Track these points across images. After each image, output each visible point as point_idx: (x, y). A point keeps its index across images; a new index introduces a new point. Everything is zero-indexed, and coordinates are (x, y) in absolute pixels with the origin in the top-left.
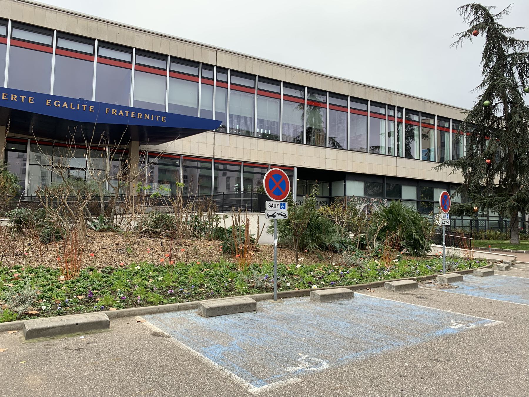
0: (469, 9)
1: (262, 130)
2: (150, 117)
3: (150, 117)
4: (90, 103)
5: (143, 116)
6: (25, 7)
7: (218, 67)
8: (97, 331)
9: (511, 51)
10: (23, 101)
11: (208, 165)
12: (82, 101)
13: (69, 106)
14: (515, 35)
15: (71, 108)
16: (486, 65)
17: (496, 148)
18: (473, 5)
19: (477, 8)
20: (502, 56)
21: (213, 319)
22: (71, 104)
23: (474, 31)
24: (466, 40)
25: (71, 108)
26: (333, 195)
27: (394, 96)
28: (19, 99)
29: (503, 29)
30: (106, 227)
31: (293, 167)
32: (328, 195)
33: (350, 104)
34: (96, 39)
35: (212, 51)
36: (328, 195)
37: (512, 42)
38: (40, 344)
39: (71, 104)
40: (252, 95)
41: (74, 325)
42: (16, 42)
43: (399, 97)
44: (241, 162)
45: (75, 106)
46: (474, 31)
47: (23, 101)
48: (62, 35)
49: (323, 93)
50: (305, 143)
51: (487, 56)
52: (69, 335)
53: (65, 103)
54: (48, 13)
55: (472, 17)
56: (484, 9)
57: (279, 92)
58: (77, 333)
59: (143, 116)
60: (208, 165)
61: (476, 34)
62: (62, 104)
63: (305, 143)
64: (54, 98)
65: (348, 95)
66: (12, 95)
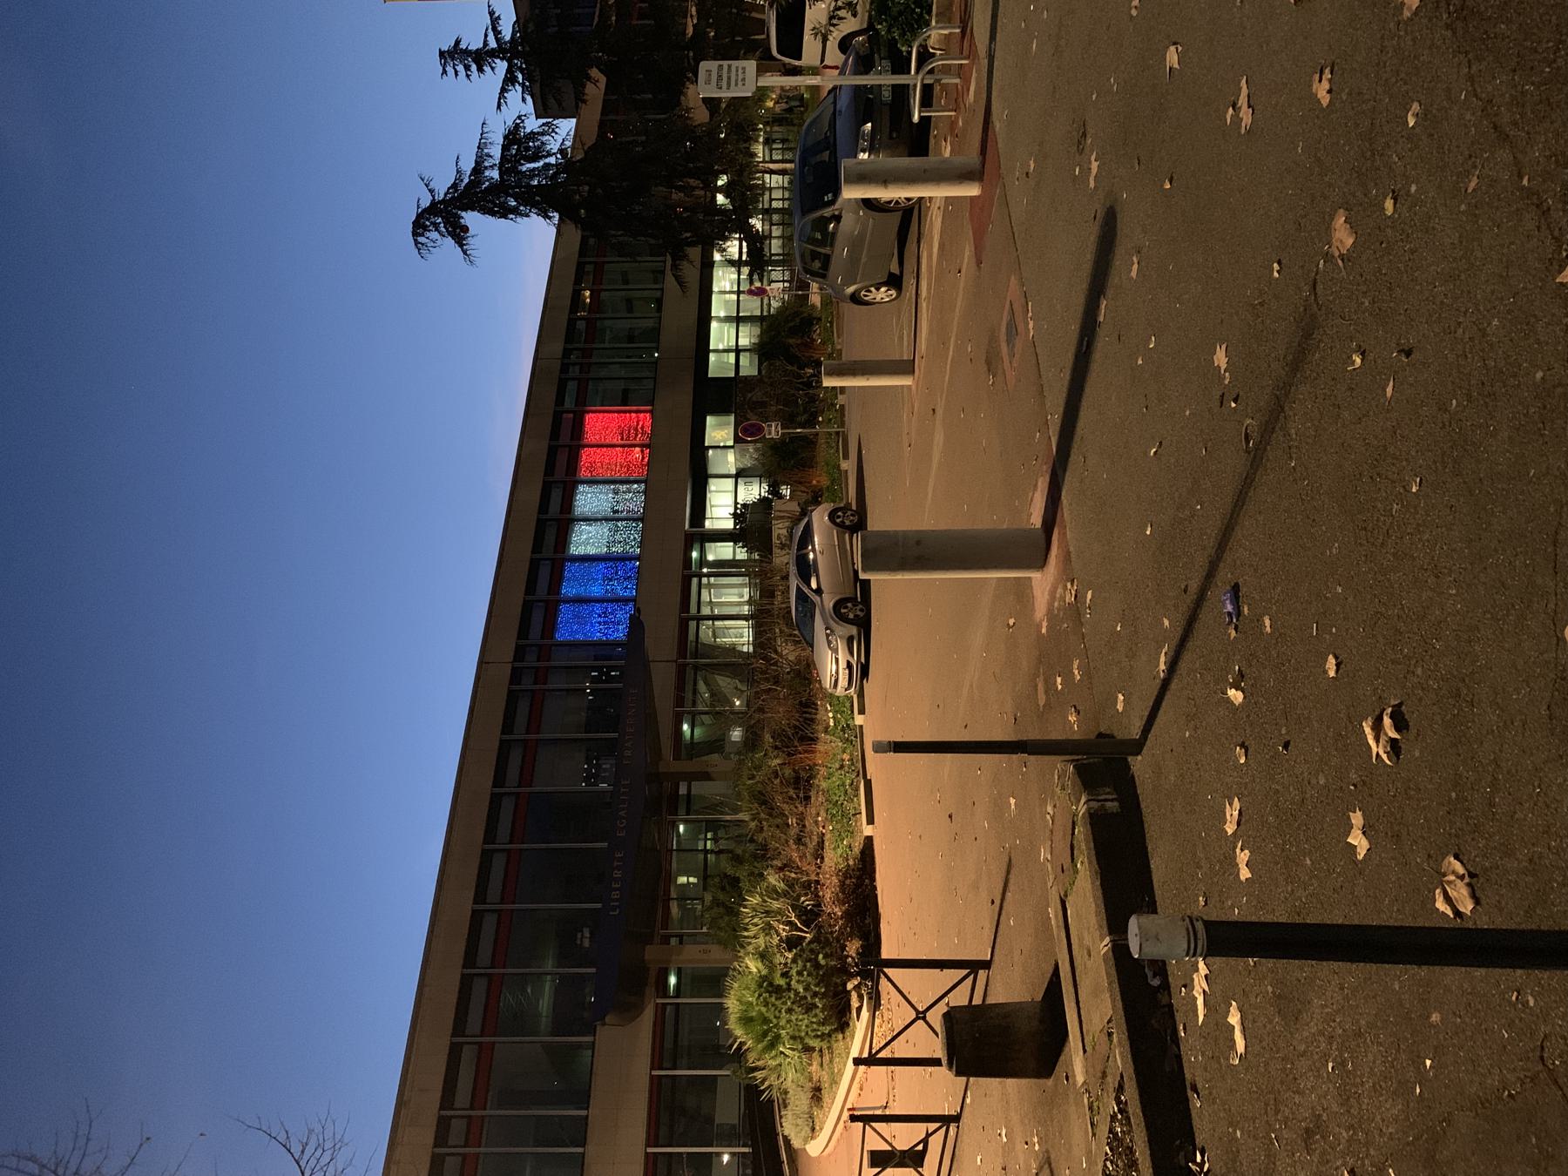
0: (421, 239)
9: (495, 174)
14: (468, 165)
16: (515, 211)
17: (549, 130)
18: (415, 234)
19: (419, 227)
20: (499, 188)
21: (913, 159)
23: (459, 234)
24: (472, 243)
26: (734, 472)
29: (454, 186)
30: (853, 948)
32: (731, 482)
36: (731, 482)
37: (478, 170)
46: (459, 234)
51: (504, 212)
55: (434, 235)
56: (419, 216)
61: (466, 229)
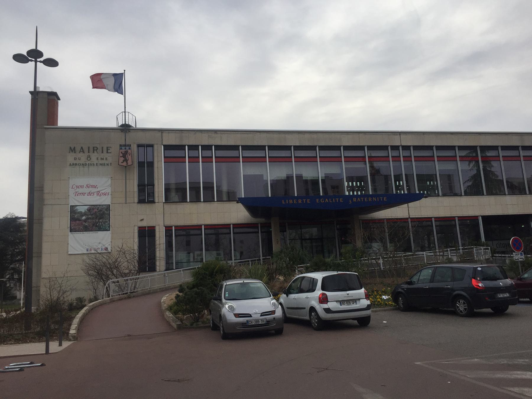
1: (359, 194)
2: (377, 199)
3: (377, 199)
5: (372, 199)
7: (403, 147)
13: (329, 201)
27: (398, 137)
31: (478, 216)
33: (522, 153)
34: (212, 146)
35: (397, 135)
40: (455, 162)
42: (505, 158)
43: (403, 136)
48: (297, 148)
49: (495, 148)
50: (485, 193)
57: (409, 155)
59: (372, 199)
63: (485, 193)
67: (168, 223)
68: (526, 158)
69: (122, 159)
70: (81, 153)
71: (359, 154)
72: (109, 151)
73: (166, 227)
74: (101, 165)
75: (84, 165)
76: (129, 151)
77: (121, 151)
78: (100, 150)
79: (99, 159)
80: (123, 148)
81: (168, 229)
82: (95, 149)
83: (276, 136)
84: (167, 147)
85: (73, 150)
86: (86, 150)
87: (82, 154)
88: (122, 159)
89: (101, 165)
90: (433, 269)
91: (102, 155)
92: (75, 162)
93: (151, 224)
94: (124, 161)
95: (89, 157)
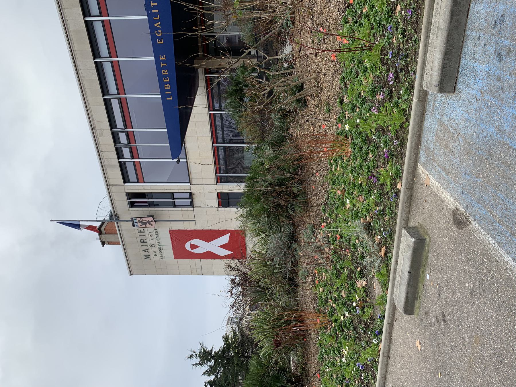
4: (157, 61)
6: (76, 49)
8: (425, 254)
10: (156, 4)
11: (220, 140)
12: (153, 29)
13: (157, 21)
15: (158, 18)
22: (154, 19)
25: (158, 18)
28: (165, 68)
38: (475, 60)
39: (154, 19)
41: (410, 276)
44: (210, 114)
45: (155, 15)
47: (156, 4)
52: (420, 280)
53: (155, 25)
54: (71, 28)
58: (421, 273)
60: (220, 140)
62: (157, 29)
64: (162, 91)
65: (94, 65)
66: (163, 74)
67: (214, 181)
68: (103, 11)
69: (148, 225)
70: (149, 251)
71: (115, 104)
72: (143, 231)
73: (217, 183)
74: (157, 237)
75: (160, 249)
76: (138, 219)
77: (139, 226)
78: (144, 238)
79: (152, 238)
80: (136, 224)
81: (219, 181)
82: (142, 241)
83: (76, 46)
84: (126, 180)
85: (147, 257)
86: (146, 248)
87: (150, 251)
88: (148, 225)
89: (157, 237)
90: (404, 231)
91: (147, 236)
92: (159, 255)
93: (216, 196)
94: (150, 224)
95: (151, 246)
